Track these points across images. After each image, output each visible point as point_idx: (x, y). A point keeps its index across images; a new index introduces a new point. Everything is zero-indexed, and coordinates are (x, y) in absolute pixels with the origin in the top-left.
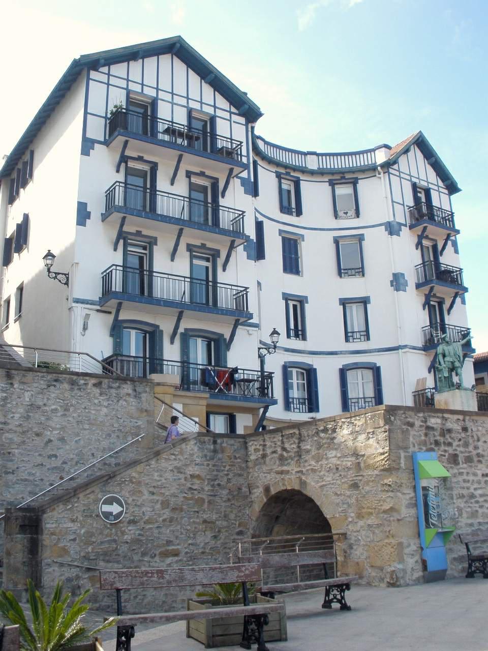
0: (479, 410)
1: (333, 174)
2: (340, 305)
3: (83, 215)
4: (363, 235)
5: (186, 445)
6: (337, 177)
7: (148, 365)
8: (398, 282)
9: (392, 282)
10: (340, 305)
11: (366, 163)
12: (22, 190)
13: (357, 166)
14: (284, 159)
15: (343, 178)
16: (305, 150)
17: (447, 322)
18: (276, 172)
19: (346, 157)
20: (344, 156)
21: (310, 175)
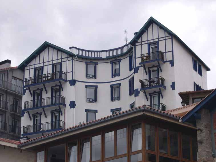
0: (77, 145)
1: (111, 58)
2: (85, 112)
3: (172, 63)
4: (97, 86)
5: (179, 161)
6: (114, 59)
7: (13, 127)
8: (73, 105)
9: (76, 106)
10: (85, 112)
11: (98, 56)
12: (97, 65)
13: (112, 56)
14: (91, 55)
15: (116, 60)
16: (101, 50)
17: (60, 119)
18: (86, 62)
19: (97, 53)
20: (98, 52)
21: (124, 56)
